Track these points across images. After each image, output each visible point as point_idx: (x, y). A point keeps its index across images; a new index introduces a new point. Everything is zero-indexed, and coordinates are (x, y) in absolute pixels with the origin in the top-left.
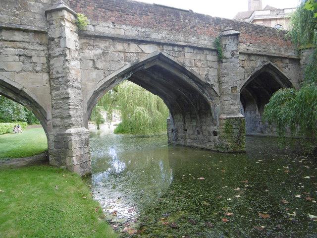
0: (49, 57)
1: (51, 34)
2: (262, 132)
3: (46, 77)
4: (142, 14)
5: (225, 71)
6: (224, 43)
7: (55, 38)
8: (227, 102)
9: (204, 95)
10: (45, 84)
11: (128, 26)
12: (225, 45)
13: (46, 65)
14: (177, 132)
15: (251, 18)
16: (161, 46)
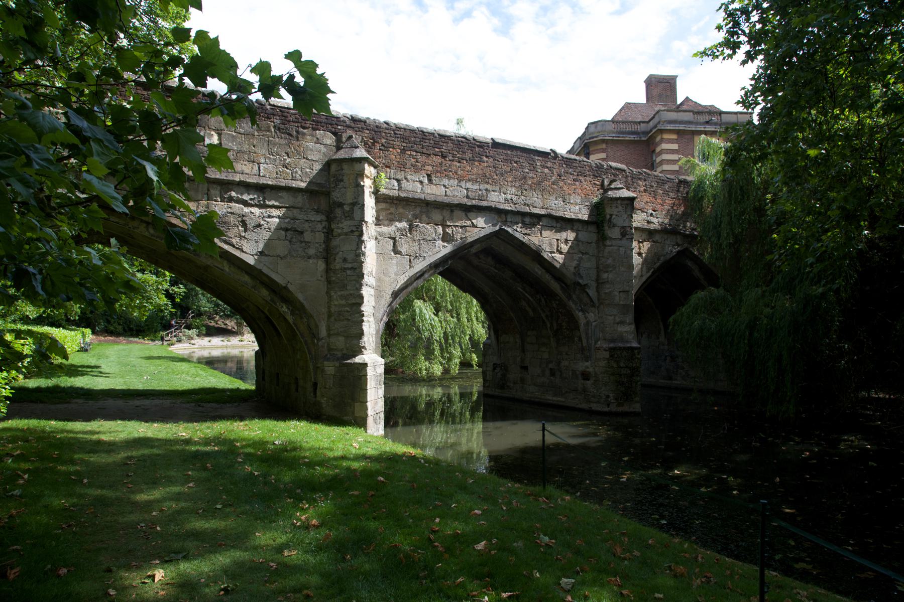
0: (329, 233)
1: (336, 196)
2: (670, 378)
3: (321, 265)
5: (610, 261)
6: (608, 211)
7: (344, 204)
8: (611, 318)
10: (320, 278)
12: (611, 215)
13: (323, 246)
15: (651, 124)
16: (503, 216)
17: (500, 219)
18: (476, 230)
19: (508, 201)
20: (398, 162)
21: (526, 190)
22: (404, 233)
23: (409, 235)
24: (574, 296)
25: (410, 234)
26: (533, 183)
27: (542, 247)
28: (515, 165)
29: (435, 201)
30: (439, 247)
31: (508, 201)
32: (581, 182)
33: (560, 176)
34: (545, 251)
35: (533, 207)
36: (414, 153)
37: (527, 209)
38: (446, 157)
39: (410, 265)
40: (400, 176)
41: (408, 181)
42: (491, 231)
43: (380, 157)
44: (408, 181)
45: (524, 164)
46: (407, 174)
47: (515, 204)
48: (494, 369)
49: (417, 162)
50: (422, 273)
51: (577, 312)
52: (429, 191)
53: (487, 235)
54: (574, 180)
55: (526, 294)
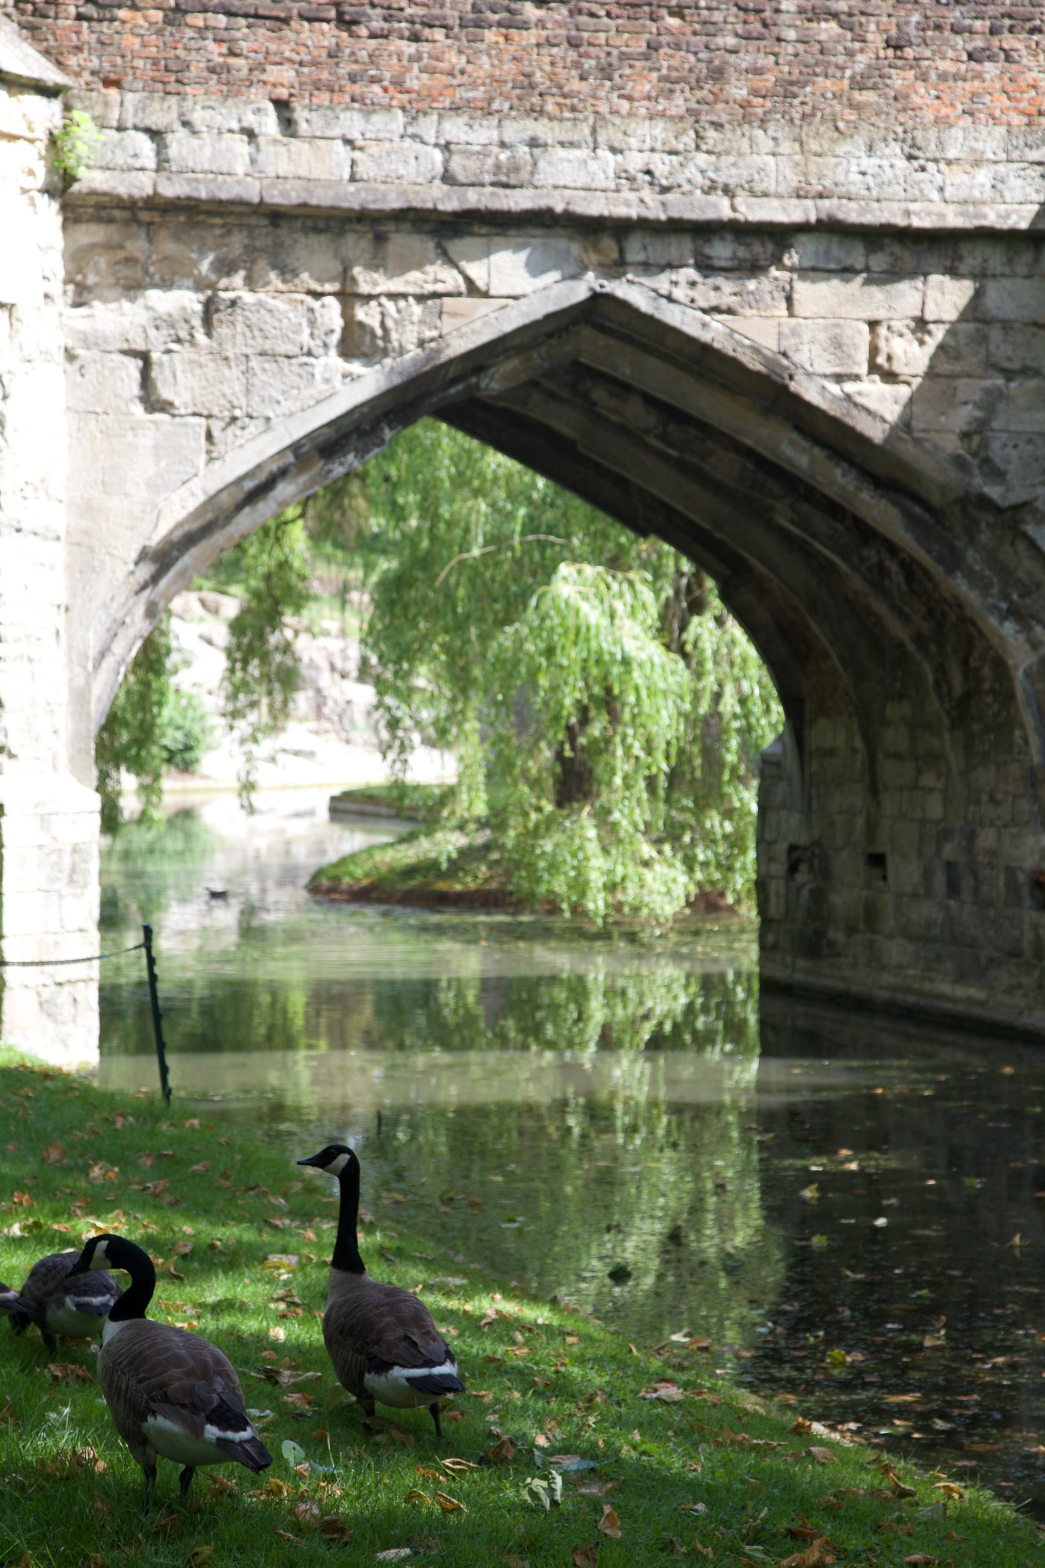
4: (478, 25)
9: (960, 585)
11: (378, 119)
14: (824, 872)
16: (608, 243)
17: (593, 258)
18: (483, 306)
19: (631, 179)
20: (155, 63)
21: (718, 126)
22: (183, 334)
23: (200, 337)
24: (971, 556)
25: (209, 334)
26: (755, 93)
27: (796, 358)
28: (673, 22)
29: (304, 205)
30: (327, 381)
31: (631, 179)
32: (1008, 59)
33: (898, 47)
34: (809, 375)
35: (752, 193)
36: (222, 20)
37: (722, 209)
38: (355, 22)
39: (208, 452)
40: (163, 114)
41: (194, 133)
42: (552, 308)
43: (79, 49)
44: (194, 133)
45: (717, 16)
46: (189, 104)
47: (665, 190)
48: (793, 869)
49: (232, 53)
50: (262, 477)
51: (993, 621)
52: (284, 167)
53: (535, 324)
54: (971, 57)
55: (818, 546)
